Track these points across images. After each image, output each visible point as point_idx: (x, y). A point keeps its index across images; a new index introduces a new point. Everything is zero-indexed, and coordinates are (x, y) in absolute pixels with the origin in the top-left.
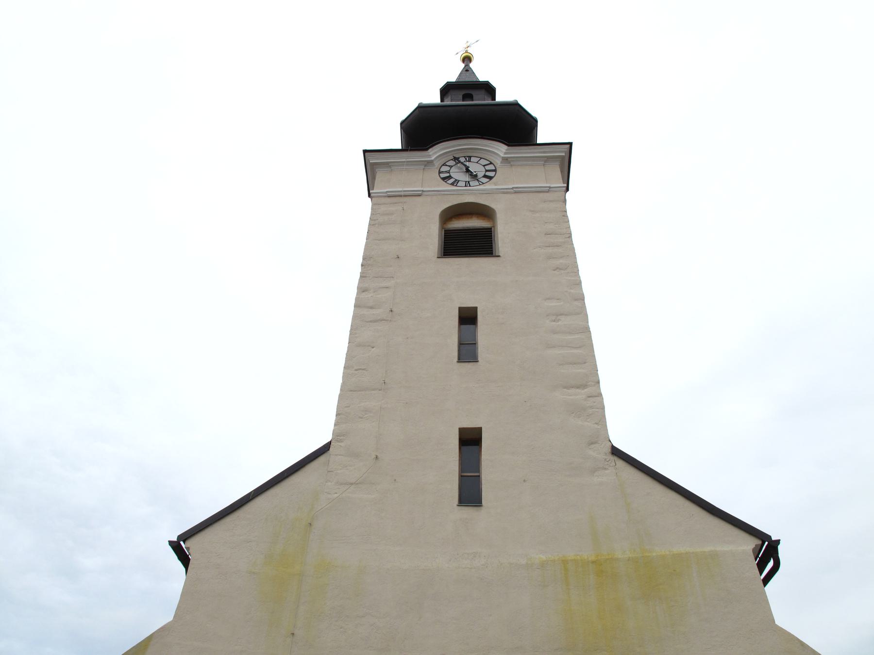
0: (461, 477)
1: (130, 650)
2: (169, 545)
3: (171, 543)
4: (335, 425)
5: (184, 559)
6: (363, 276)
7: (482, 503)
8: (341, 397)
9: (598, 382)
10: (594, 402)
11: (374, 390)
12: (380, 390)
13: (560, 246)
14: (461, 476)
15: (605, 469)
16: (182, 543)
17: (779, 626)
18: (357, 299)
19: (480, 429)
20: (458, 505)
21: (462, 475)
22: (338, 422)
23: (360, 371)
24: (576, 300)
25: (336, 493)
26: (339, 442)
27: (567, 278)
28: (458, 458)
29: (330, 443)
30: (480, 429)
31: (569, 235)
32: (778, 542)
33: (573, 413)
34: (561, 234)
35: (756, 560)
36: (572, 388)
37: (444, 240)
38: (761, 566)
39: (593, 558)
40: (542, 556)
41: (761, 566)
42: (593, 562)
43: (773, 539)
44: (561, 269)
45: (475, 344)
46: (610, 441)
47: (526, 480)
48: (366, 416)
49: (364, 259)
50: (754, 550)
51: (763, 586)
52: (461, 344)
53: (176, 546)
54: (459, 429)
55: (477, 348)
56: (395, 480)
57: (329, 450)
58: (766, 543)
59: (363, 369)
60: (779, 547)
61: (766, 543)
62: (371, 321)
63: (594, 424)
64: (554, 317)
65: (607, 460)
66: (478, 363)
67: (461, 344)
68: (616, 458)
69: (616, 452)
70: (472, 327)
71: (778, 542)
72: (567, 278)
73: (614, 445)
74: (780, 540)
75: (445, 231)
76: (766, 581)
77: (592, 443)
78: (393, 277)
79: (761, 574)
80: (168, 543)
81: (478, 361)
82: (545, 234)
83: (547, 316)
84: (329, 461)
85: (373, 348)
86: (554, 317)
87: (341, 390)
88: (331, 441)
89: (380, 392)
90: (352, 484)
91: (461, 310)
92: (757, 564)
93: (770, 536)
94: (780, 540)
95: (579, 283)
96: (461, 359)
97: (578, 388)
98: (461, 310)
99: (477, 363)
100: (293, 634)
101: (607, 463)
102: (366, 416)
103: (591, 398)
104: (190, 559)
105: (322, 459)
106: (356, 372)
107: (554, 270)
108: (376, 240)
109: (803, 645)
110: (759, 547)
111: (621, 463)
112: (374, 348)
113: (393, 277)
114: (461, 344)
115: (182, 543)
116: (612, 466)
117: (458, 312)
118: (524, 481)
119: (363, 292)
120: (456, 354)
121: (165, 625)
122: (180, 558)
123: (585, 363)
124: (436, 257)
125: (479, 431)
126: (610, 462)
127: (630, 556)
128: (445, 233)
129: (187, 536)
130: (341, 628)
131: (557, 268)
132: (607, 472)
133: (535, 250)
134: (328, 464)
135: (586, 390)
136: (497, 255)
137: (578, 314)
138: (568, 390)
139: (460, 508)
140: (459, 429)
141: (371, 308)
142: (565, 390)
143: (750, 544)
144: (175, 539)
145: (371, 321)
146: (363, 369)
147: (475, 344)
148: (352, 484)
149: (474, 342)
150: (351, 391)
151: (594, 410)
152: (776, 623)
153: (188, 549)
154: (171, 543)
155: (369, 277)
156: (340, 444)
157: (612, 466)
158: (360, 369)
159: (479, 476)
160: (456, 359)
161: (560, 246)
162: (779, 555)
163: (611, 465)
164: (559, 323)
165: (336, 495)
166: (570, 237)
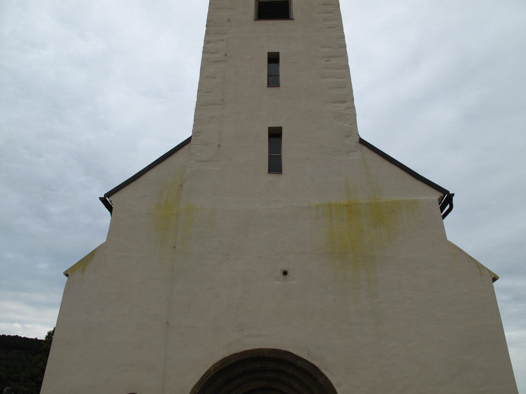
0: (270, 157)
1: (84, 258)
2: (100, 200)
3: (101, 199)
4: (194, 126)
5: (109, 207)
6: (207, 33)
7: (282, 172)
8: (196, 110)
9: (353, 100)
10: (350, 112)
11: (216, 105)
12: (220, 105)
13: (332, 12)
14: (270, 156)
15: (356, 152)
16: (107, 198)
17: (449, 240)
18: (204, 48)
19: (281, 128)
20: (268, 173)
21: (270, 155)
22: (195, 125)
23: (207, 93)
24: (341, 48)
25: (196, 167)
26: (196, 136)
27: (336, 34)
28: (268, 145)
29: (190, 138)
30: (281, 128)
31: (337, 5)
32: (453, 195)
33: (337, 118)
34: (333, 5)
35: (439, 205)
36: (337, 103)
37: (258, 9)
38: (442, 209)
39: (346, 203)
40: (317, 202)
41: (442, 209)
42: (346, 205)
43: (451, 193)
44: (332, 28)
45: (278, 75)
46: (359, 135)
47: (308, 158)
48: (212, 121)
49: (207, 22)
50: (439, 199)
51: (441, 213)
52: (269, 76)
53: (103, 200)
54: (268, 127)
55: (279, 78)
56: (231, 159)
57: (190, 141)
58: (446, 195)
59: (209, 92)
60: (453, 198)
61: (446, 195)
62: (213, 62)
63: (349, 125)
64: (327, 59)
65: (357, 146)
66: (280, 88)
67: (269, 76)
68: (362, 145)
69: (362, 142)
70: (276, 64)
71: (453, 195)
72: (336, 34)
73: (361, 137)
74: (454, 194)
75: (259, 2)
76: (444, 216)
77: (349, 136)
78: (226, 33)
79: (442, 213)
80: (99, 198)
81: (280, 86)
82: (323, 5)
83: (323, 58)
84: (191, 148)
85: (215, 78)
86: (327, 59)
87: (196, 105)
88: (191, 136)
89: (220, 106)
90: (205, 161)
91: (269, 54)
92: (440, 207)
93: (449, 192)
94: (454, 194)
95: (343, 37)
96: (269, 85)
97: (340, 103)
98: (269, 54)
99: (279, 87)
100: (175, 247)
101: (356, 148)
102: (212, 121)
103: (348, 109)
104: (112, 207)
105: (186, 147)
106: (205, 94)
107: (328, 28)
108: (214, 9)
109: (461, 251)
110: (442, 198)
111: (364, 148)
112: (216, 79)
113: (226, 33)
114: (269, 76)
115: (107, 198)
116: (360, 150)
117: (267, 55)
118: (307, 158)
119: (208, 43)
120: (266, 82)
121: (102, 244)
122: (106, 207)
123: (345, 87)
124: (253, 19)
125: (278, 54)
126: (358, 147)
127: (368, 202)
128: (259, 4)
129: (110, 194)
130: (202, 243)
131: (330, 27)
132: (356, 153)
133: (316, 15)
134: (190, 150)
135: (345, 104)
136: (292, 18)
137: (342, 57)
138: (334, 104)
139: (269, 174)
140: (268, 127)
141: (213, 53)
142: (333, 104)
143: (437, 195)
144: (103, 196)
145: (213, 62)
146: (209, 92)
147: (278, 75)
148: (205, 161)
149: (277, 75)
150: (203, 105)
151: (350, 116)
152: (448, 239)
153: (111, 201)
154: (101, 199)
155: (211, 33)
156: (197, 138)
157: (360, 150)
158: (208, 92)
159: (280, 156)
160: (266, 85)
161: (332, 12)
162: (453, 202)
163: (359, 149)
164: (330, 62)
165: (196, 168)
166: (339, 6)
